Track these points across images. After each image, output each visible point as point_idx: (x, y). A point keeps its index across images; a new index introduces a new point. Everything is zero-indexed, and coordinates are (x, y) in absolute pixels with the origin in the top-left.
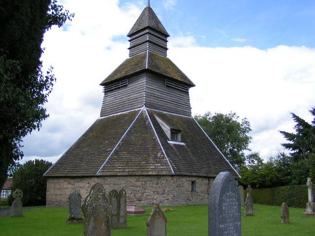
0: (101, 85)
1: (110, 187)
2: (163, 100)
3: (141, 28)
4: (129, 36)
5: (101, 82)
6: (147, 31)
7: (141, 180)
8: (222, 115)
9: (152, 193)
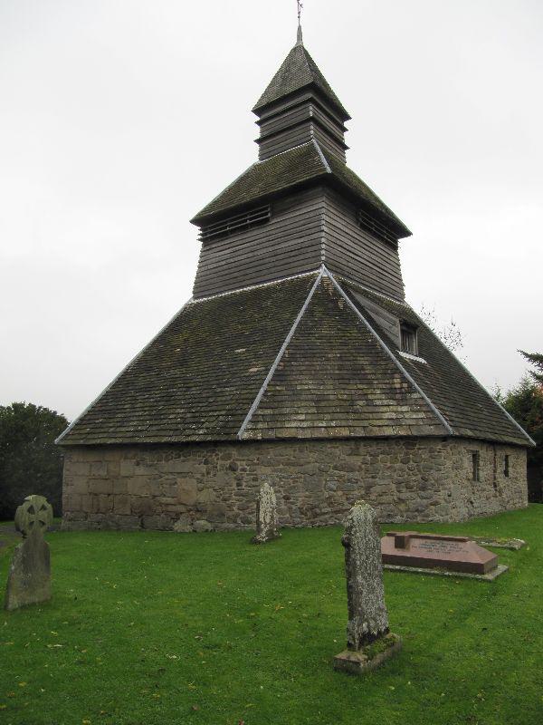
0: (195, 221)
1: (275, 471)
2: (357, 258)
3: (289, 90)
4: (257, 111)
5: (193, 215)
6: (310, 95)
7: (362, 450)
8: (21, 406)
9: (394, 486)
